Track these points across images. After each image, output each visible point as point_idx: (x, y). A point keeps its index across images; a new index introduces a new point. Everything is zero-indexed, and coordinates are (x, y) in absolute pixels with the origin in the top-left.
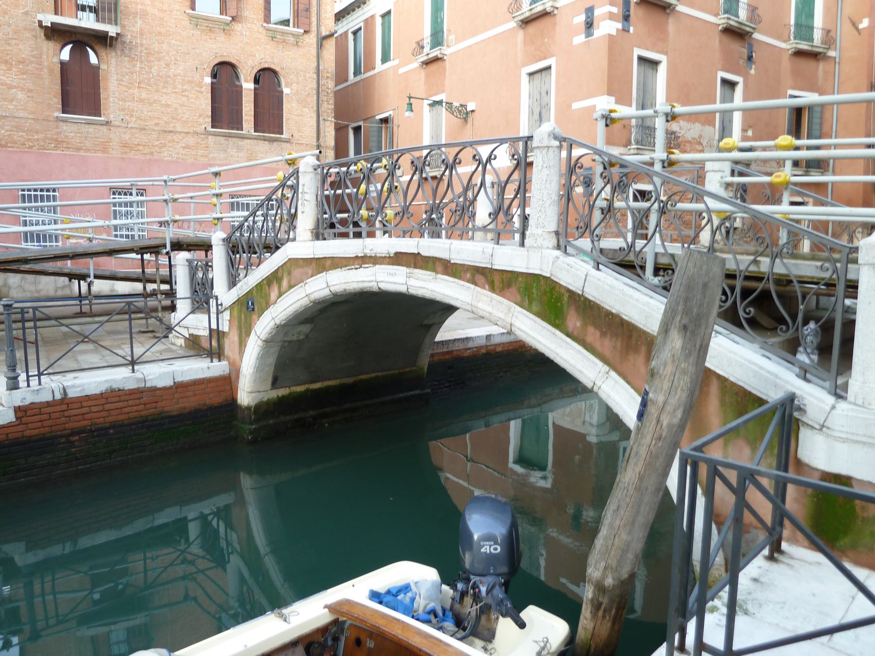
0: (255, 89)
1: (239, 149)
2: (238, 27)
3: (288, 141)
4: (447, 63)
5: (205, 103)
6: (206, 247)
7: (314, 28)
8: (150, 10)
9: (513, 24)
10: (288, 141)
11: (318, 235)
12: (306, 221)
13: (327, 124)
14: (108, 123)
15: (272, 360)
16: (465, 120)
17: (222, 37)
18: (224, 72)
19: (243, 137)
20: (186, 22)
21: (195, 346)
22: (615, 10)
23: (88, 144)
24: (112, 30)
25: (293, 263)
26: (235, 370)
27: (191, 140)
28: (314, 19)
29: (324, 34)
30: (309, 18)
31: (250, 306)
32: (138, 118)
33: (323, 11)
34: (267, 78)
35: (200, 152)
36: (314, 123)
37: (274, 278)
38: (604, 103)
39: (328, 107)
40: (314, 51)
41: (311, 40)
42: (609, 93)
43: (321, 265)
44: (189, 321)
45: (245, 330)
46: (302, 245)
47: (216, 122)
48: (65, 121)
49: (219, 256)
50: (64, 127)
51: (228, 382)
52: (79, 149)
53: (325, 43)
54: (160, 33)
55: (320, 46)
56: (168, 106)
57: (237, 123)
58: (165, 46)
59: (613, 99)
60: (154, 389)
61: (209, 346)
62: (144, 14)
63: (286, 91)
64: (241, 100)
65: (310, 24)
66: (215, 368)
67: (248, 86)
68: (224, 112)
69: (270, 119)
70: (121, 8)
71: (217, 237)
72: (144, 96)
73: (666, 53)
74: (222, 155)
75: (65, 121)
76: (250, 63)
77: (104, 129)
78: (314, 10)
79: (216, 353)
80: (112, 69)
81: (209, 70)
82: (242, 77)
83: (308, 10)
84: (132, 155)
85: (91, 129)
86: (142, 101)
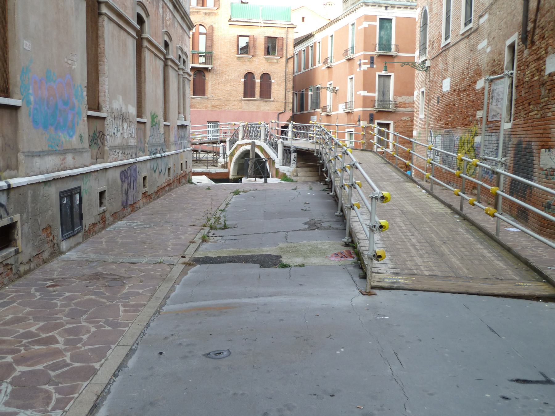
0: (261, 81)
1: (254, 105)
2: (254, 59)
3: (273, 101)
4: (333, 69)
5: (241, 89)
6: (225, 142)
7: (285, 55)
8: (223, 57)
9: (344, 60)
10: (273, 101)
11: (243, 139)
12: (240, 136)
13: (289, 93)
14: (207, 98)
15: (237, 168)
16: (336, 93)
17: (248, 63)
18: (249, 76)
19: (255, 101)
20: (235, 59)
21: (223, 166)
22: (366, 61)
23: (201, 106)
24: (210, 67)
25: (238, 145)
26: (229, 170)
27: (236, 103)
28: (285, 52)
29: (289, 57)
30: (282, 52)
31: (232, 155)
32: (218, 96)
33: (288, 48)
34: (266, 77)
35: (239, 107)
36: (284, 93)
37: (235, 149)
38: (364, 93)
39: (290, 86)
40: (284, 64)
41: (284, 60)
42: (364, 90)
43: (242, 145)
44: (221, 160)
45: (231, 160)
46: (240, 142)
47: (245, 95)
48: (194, 98)
49: (228, 144)
50: (194, 101)
51: (228, 174)
52: (198, 108)
53: (289, 60)
54: (226, 65)
55: (287, 62)
56: (228, 91)
57: (253, 95)
58: (228, 69)
59: (366, 92)
60: (211, 173)
61: (224, 166)
62: (221, 58)
63: (273, 81)
64: (256, 87)
65: (283, 54)
66: (225, 170)
67: (258, 81)
68: (249, 92)
69: (266, 92)
70: (213, 57)
71: (228, 140)
72: (220, 88)
73: (393, 72)
74: (247, 108)
75: (194, 98)
76: (259, 72)
77: (206, 100)
78: (285, 48)
79: (226, 167)
80: (210, 79)
81: (243, 76)
82: (256, 78)
83: (282, 49)
84: (215, 109)
85: (202, 101)
86: (219, 89)
